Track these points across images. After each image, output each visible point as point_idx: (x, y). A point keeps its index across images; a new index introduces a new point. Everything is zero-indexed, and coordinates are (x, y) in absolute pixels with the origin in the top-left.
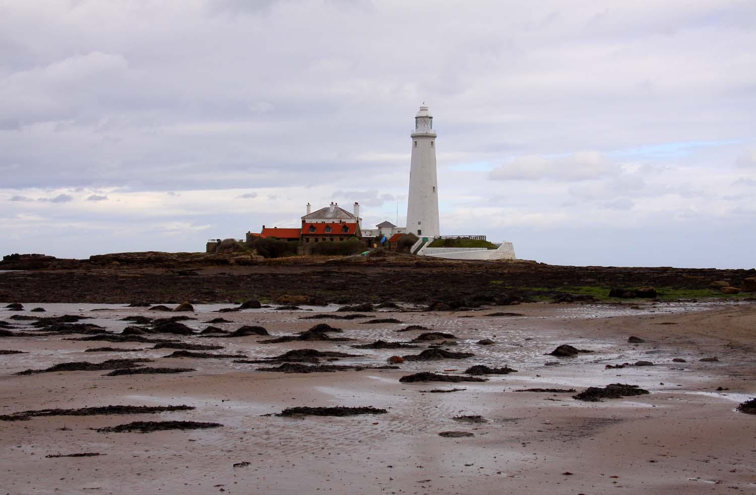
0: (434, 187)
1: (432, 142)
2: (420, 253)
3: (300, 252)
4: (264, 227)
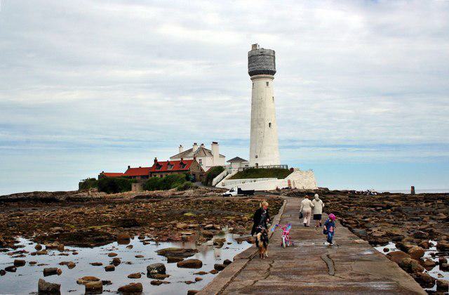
0: (270, 124)
1: (267, 83)
2: (217, 186)
3: (133, 188)
4: (129, 167)
